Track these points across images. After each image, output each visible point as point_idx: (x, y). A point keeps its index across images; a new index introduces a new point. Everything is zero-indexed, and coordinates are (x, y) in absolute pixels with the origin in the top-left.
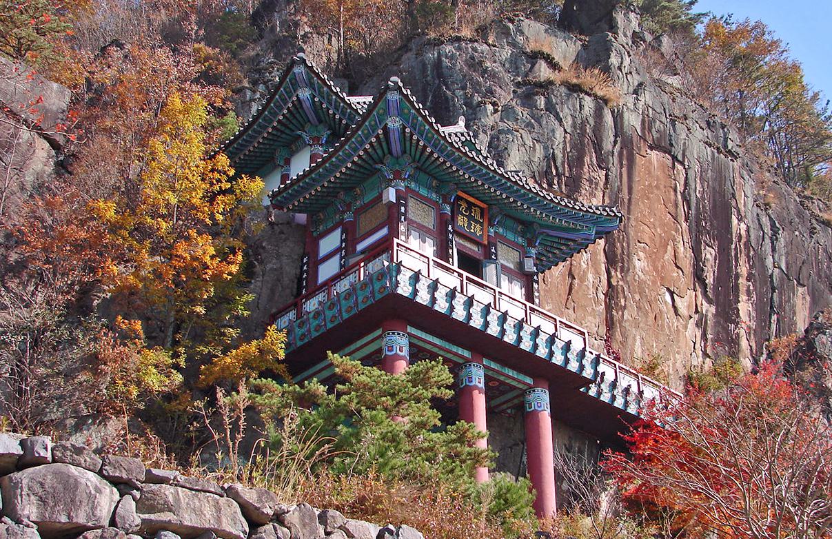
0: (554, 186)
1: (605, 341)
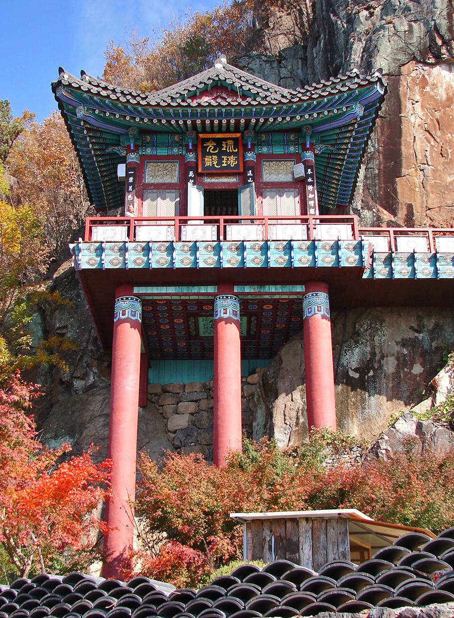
0: (444, 56)
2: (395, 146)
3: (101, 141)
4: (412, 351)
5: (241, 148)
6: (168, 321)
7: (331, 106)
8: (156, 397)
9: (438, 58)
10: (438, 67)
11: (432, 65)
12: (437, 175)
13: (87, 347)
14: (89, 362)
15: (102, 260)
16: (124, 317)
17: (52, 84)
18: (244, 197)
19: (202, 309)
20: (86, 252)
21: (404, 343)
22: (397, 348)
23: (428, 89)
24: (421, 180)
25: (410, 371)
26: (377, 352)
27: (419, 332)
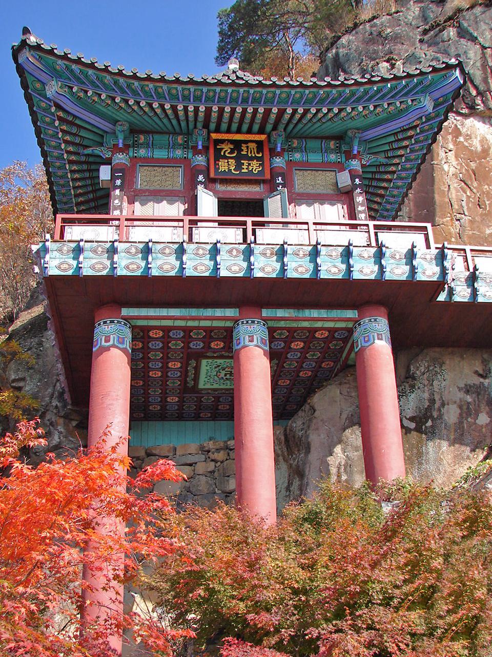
0: (478, 107)
2: (427, 193)
3: (78, 140)
4: (476, 399)
5: (267, 152)
6: (160, 365)
7: (392, 97)
8: (139, 461)
9: (472, 107)
10: (472, 119)
11: (466, 116)
12: (475, 226)
13: (51, 402)
14: (53, 420)
15: (79, 263)
16: (108, 344)
17: (13, 47)
18: (274, 205)
19: (209, 347)
20: (56, 254)
21: (468, 390)
22: (461, 395)
23: (461, 139)
24: (458, 230)
25: (475, 421)
26: (436, 399)
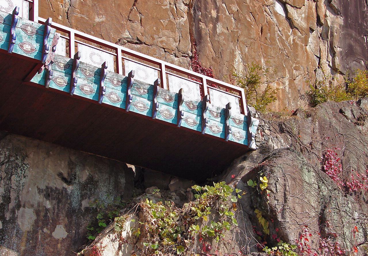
1: (191, 58)
22: (39, 198)
24: (66, 9)
25: (51, 233)
27: (69, 183)
